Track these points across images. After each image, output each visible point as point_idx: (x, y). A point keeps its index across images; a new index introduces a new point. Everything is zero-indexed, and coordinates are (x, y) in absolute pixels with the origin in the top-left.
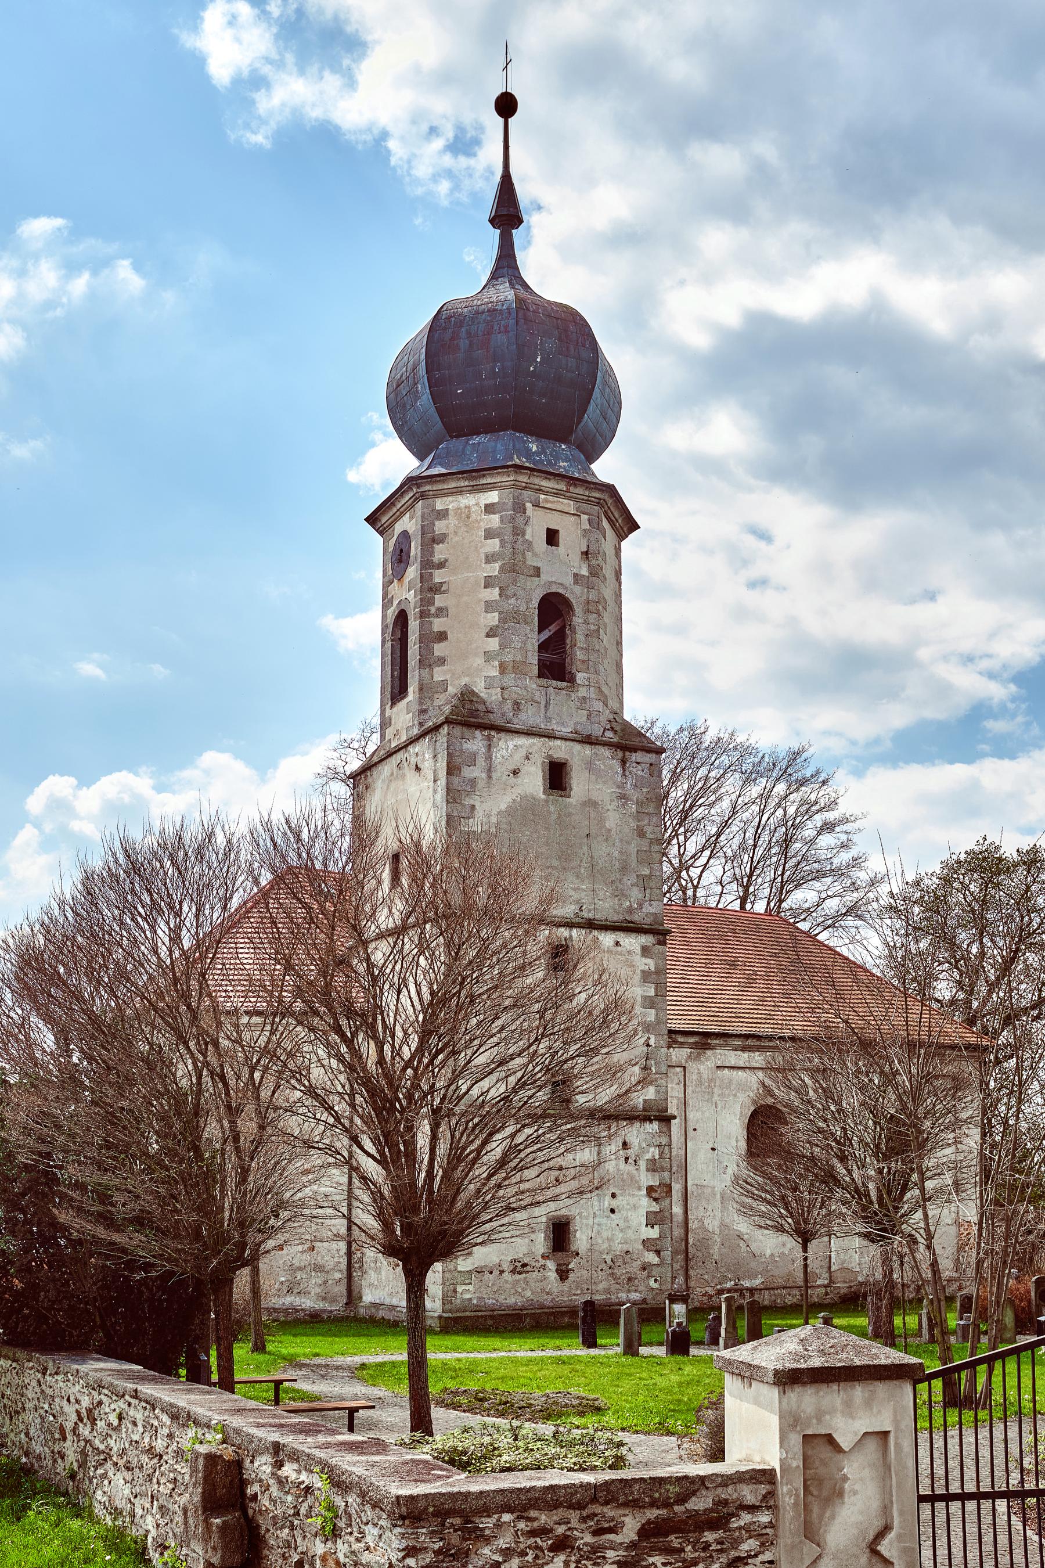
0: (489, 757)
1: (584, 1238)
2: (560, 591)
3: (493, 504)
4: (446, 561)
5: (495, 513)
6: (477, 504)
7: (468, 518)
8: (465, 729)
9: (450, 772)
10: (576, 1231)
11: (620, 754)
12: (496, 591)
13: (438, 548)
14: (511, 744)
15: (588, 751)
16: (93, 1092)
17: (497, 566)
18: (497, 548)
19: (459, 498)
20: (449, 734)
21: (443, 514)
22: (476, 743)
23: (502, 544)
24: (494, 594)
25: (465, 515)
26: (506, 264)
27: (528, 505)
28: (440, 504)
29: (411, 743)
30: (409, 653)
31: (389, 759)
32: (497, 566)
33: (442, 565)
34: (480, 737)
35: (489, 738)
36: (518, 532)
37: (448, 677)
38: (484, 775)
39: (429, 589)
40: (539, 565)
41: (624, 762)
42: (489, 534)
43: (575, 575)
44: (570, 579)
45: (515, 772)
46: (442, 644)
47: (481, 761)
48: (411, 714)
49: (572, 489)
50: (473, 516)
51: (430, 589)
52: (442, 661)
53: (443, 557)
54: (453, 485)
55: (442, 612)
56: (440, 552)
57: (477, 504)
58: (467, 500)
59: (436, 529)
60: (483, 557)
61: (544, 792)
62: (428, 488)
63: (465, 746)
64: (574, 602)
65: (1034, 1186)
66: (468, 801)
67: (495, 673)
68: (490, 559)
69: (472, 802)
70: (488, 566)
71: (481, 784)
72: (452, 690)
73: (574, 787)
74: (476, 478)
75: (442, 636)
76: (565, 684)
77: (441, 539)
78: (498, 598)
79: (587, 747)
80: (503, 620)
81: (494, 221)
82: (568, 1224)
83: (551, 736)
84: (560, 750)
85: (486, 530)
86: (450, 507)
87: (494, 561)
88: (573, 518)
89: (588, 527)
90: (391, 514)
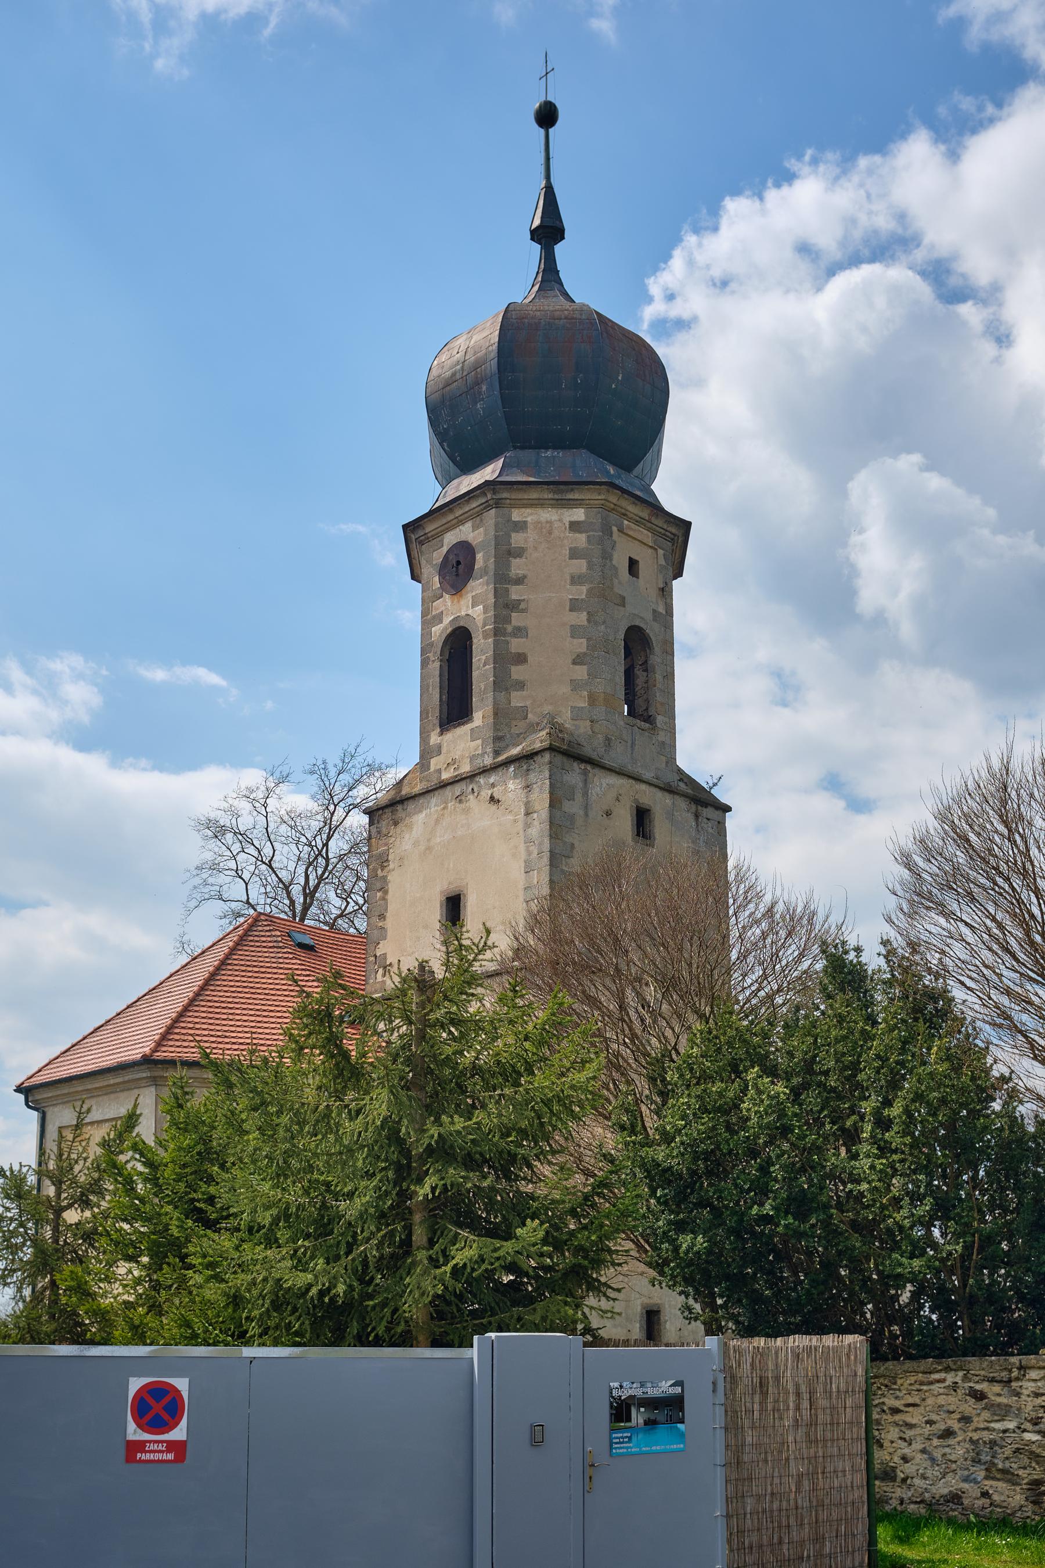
0: (585, 794)
1: (673, 1329)
2: (642, 625)
3: (578, 523)
4: (525, 577)
5: (580, 532)
6: (560, 520)
7: (550, 533)
8: (565, 759)
9: (552, 805)
10: (666, 1322)
11: (693, 806)
12: (584, 616)
13: (515, 562)
14: (603, 781)
15: (668, 799)
17: (584, 589)
18: (584, 570)
19: (540, 511)
20: (550, 763)
21: (521, 526)
22: (574, 775)
23: (590, 566)
24: (582, 618)
25: (546, 530)
26: (549, 275)
27: (615, 529)
28: (516, 515)
29: (484, 771)
31: (440, 791)
32: (584, 589)
33: (520, 581)
34: (578, 771)
35: (585, 773)
36: (607, 556)
37: (528, 703)
38: (582, 812)
39: (504, 607)
40: (625, 594)
41: (697, 816)
42: (574, 554)
43: (654, 611)
44: (649, 616)
45: (608, 814)
46: (521, 668)
47: (579, 796)
48: (479, 742)
49: (653, 520)
50: (556, 533)
51: (506, 606)
52: (521, 685)
53: (521, 572)
54: (535, 496)
55: (520, 632)
56: (517, 567)
57: (560, 520)
58: (547, 515)
59: (513, 541)
60: (568, 578)
61: (633, 839)
62: (505, 495)
63: (565, 777)
64: (653, 639)
65: (882, 1292)
66: (568, 839)
67: (583, 704)
68: (576, 580)
69: (571, 840)
70: (574, 588)
71: (579, 821)
73: (657, 836)
74: (562, 492)
75: (521, 659)
76: (647, 725)
77: (519, 553)
78: (586, 623)
79: (666, 794)
80: (592, 647)
81: (536, 235)
82: (658, 1312)
83: (638, 779)
84: (649, 796)
85: (570, 549)
86: (529, 519)
87: (581, 584)
88: (650, 551)
89: (664, 563)
90: (444, 521)
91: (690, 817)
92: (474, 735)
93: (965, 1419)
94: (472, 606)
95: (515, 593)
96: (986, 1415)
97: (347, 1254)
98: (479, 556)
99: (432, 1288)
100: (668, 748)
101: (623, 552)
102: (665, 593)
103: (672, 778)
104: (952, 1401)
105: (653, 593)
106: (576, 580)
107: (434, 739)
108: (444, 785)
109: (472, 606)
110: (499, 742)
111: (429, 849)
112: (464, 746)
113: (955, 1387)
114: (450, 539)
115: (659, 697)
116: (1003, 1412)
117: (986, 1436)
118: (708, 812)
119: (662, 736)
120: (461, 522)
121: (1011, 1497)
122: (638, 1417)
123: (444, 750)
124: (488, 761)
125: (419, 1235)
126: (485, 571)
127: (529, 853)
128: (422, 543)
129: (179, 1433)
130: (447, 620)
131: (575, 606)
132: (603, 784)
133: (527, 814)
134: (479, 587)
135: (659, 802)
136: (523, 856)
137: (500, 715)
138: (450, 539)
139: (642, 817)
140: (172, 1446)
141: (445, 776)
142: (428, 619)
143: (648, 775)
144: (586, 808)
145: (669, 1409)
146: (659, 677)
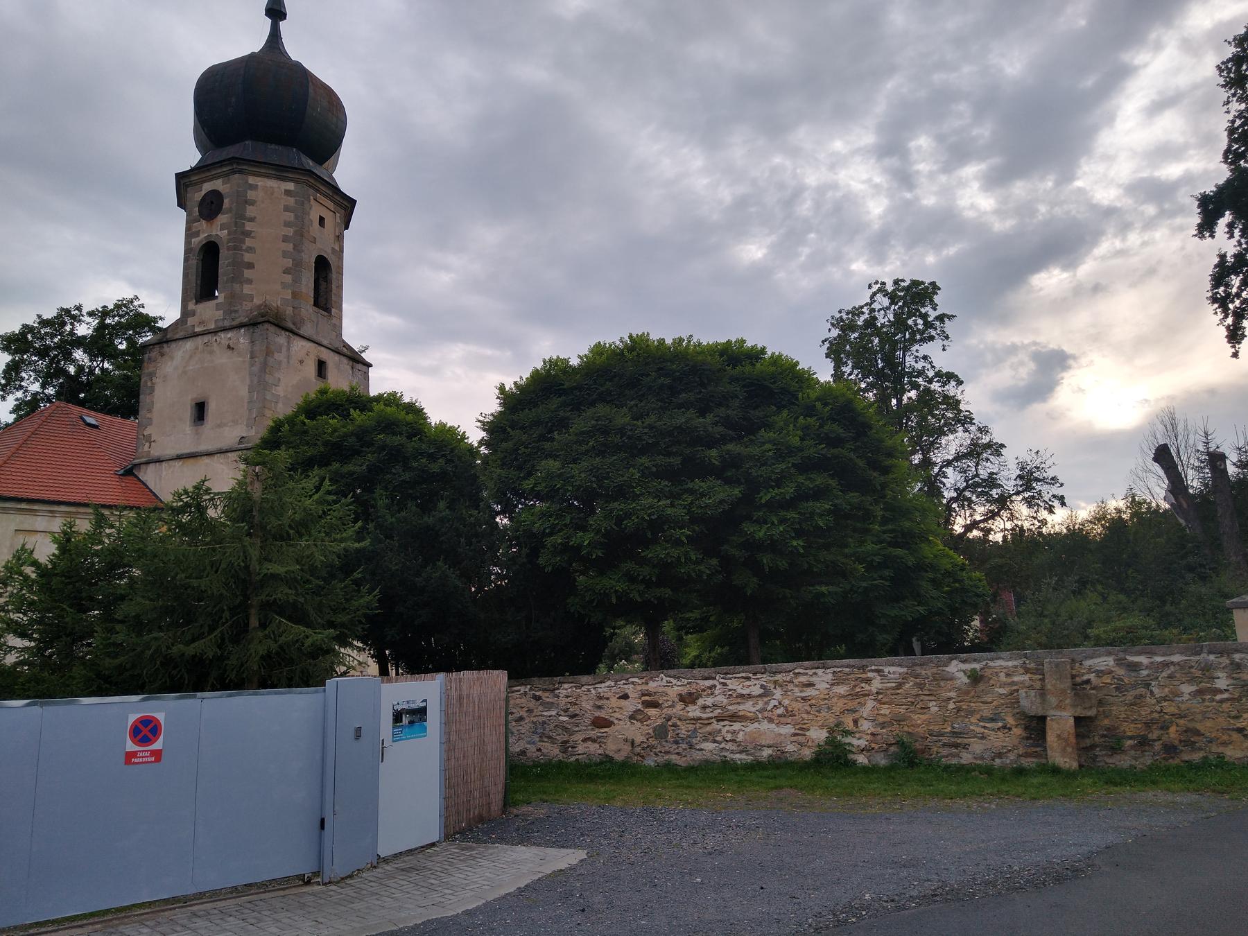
13: (249, 208)
15: (336, 357)
16: (511, 547)
21: (254, 187)
23: (296, 217)
28: (251, 180)
30: (220, 271)
33: (252, 220)
35: (289, 337)
44: (330, 251)
45: (301, 362)
47: (284, 350)
52: (250, 281)
53: (253, 215)
56: (250, 211)
58: (272, 183)
66: (277, 375)
68: (287, 224)
72: (257, 301)
77: (253, 203)
91: (349, 367)
92: (218, 307)
93: (530, 711)
94: (218, 230)
95: (249, 226)
96: (541, 708)
97: (209, 634)
98: (226, 201)
99: (262, 650)
100: (338, 328)
101: (316, 211)
102: (340, 238)
103: (337, 345)
104: (523, 701)
105: (332, 237)
106: (287, 224)
107: (191, 306)
108: (196, 335)
109: (218, 230)
110: (230, 310)
111: (185, 372)
112: (209, 312)
113: (525, 694)
114: (207, 187)
115: (334, 298)
116: (550, 706)
117: (541, 719)
118: (360, 366)
119: (334, 321)
120: (215, 178)
121: (882, 761)
122: (405, 720)
123: (197, 314)
124: (227, 324)
125: (254, 622)
126: (230, 210)
127: (252, 381)
128: (187, 186)
129: (157, 745)
130: (202, 236)
131: (285, 239)
132: (299, 346)
133: (252, 358)
134: (222, 218)
135: (331, 359)
136: (248, 382)
137: (233, 298)
138: (207, 187)
139: (321, 366)
140: (153, 753)
141: (197, 330)
142: (190, 234)
143: (325, 342)
144: (288, 357)
145: (419, 714)
146: (334, 287)
